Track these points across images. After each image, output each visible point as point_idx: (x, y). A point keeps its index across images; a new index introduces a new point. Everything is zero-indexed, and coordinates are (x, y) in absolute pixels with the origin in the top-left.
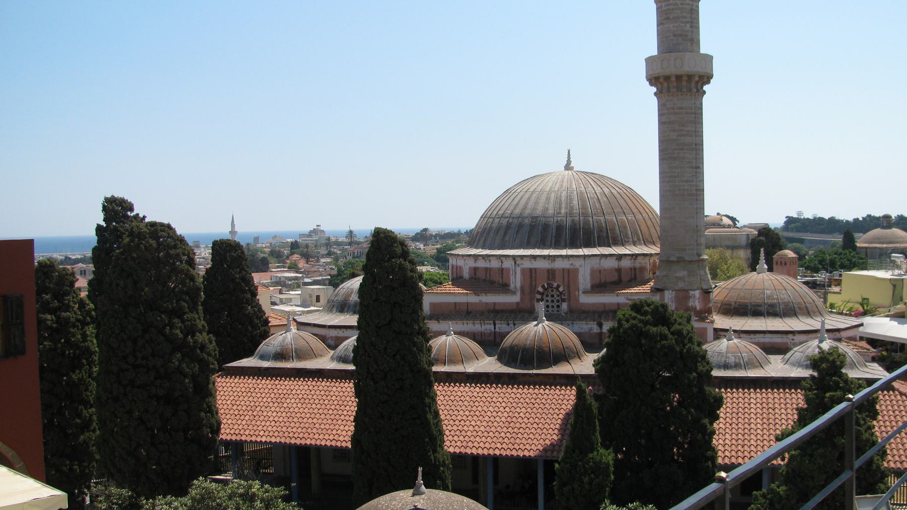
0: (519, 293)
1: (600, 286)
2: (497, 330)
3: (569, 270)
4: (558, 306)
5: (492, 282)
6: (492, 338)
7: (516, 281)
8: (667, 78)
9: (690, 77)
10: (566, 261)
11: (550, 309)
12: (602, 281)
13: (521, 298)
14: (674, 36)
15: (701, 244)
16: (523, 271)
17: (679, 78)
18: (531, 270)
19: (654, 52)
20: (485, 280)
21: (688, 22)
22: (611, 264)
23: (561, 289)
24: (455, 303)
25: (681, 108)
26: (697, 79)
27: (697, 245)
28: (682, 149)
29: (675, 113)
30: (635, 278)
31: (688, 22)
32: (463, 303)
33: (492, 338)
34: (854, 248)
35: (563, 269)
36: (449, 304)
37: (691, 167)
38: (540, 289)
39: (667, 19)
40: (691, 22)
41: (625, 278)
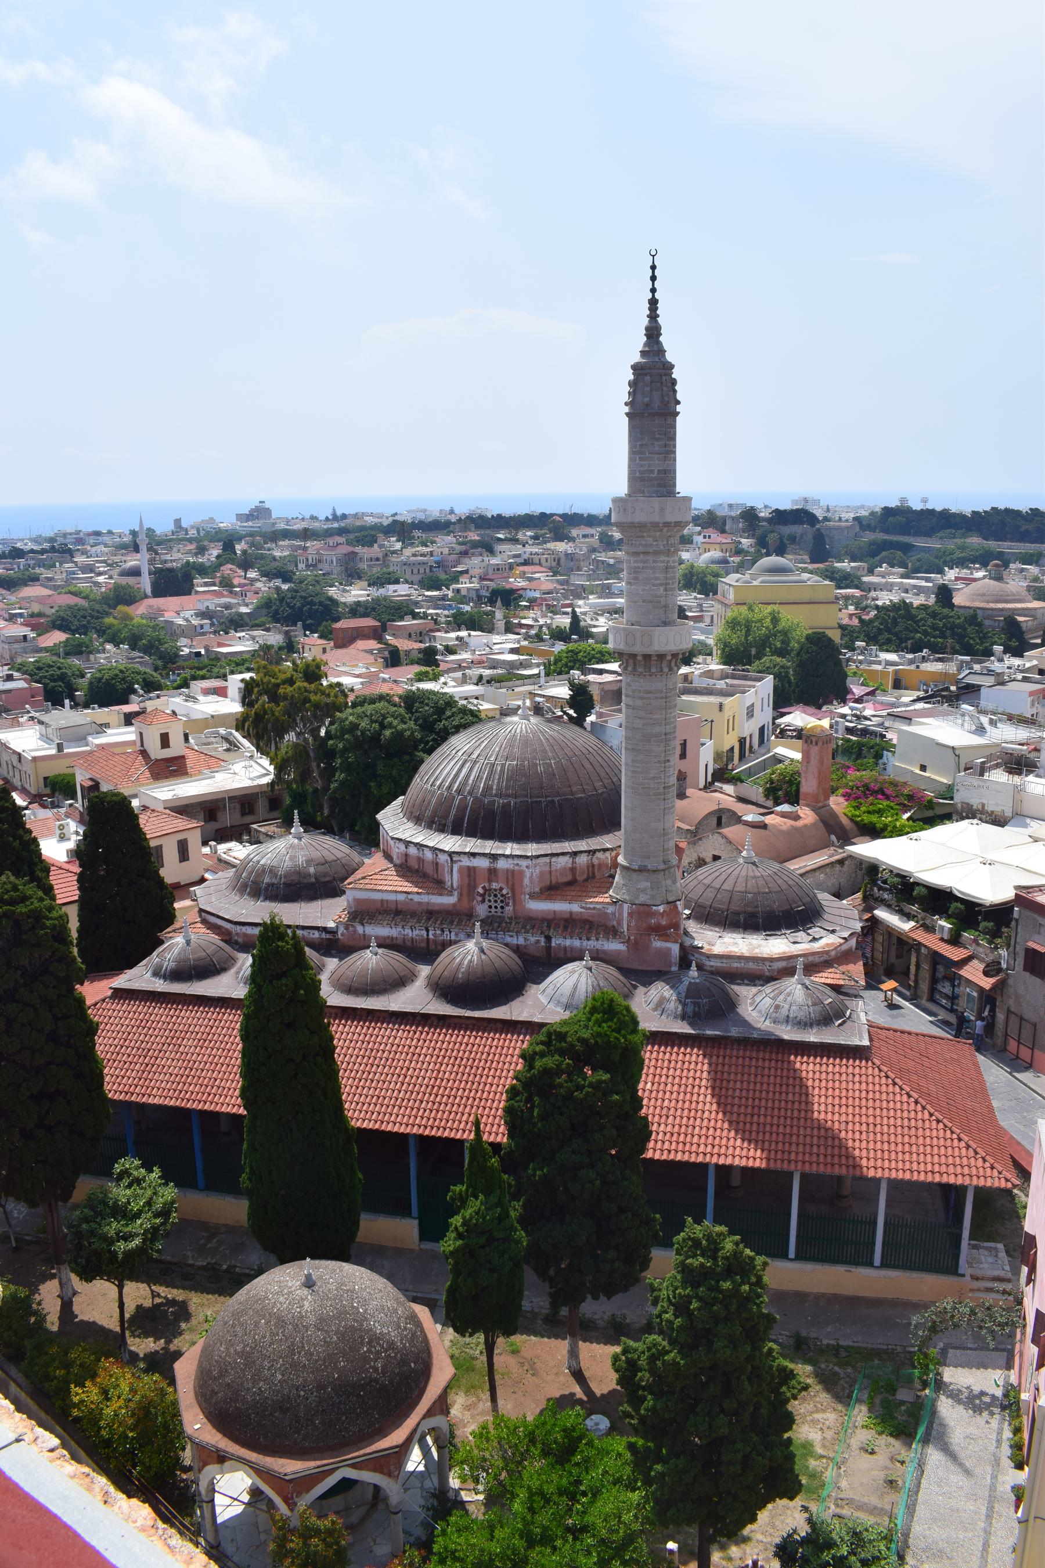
0: (456, 893)
1: (551, 890)
2: (431, 936)
3: (513, 872)
4: (502, 907)
5: (425, 876)
6: (423, 945)
7: (455, 879)
8: (633, 656)
9: (661, 657)
10: (510, 861)
11: (493, 910)
12: (554, 882)
13: (459, 900)
14: (644, 601)
15: (668, 849)
16: (461, 870)
17: (647, 657)
18: (469, 868)
19: (632, 377)
20: (417, 871)
21: (661, 585)
22: (564, 862)
23: (504, 892)
24: (382, 900)
25: (650, 692)
26: (669, 658)
27: (664, 850)
28: (649, 741)
29: (642, 698)
30: (594, 876)
31: (661, 585)
32: (391, 901)
33: (423, 945)
34: (952, 606)
35: (507, 870)
36: (374, 901)
37: (659, 762)
38: (481, 891)
39: (636, 578)
40: (666, 584)
41: (580, 878)
